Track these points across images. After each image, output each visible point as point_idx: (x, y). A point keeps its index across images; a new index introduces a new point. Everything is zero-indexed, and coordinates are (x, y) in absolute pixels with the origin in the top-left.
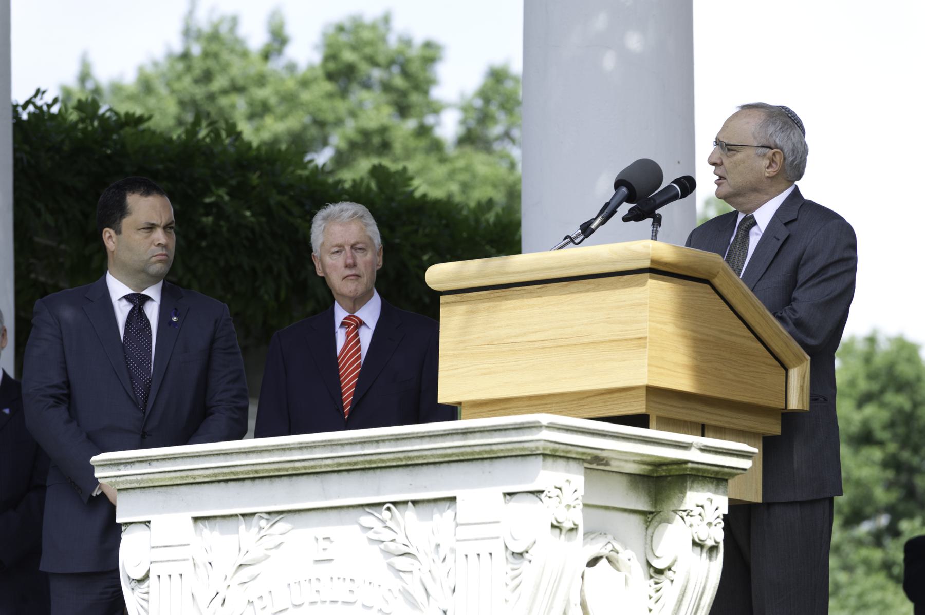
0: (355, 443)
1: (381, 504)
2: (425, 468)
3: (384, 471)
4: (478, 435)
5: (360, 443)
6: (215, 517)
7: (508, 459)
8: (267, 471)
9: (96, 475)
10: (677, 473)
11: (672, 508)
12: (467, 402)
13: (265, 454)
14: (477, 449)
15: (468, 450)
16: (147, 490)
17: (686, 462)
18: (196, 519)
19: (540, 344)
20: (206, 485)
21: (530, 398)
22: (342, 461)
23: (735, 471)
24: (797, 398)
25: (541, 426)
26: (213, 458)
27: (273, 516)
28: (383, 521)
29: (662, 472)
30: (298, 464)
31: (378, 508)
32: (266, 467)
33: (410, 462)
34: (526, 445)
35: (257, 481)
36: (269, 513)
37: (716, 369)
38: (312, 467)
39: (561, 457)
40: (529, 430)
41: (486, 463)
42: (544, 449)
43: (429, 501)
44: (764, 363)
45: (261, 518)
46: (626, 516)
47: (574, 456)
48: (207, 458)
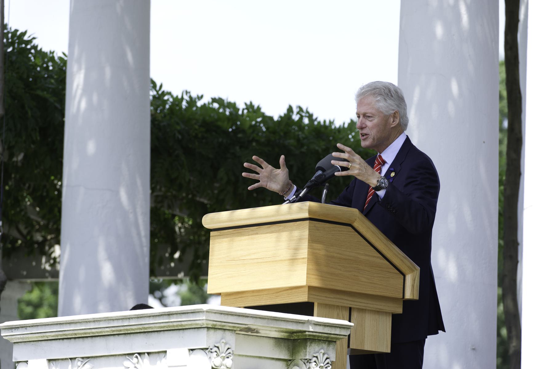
0: (119, 319)
1: (133, 354)
2: (153, 333)
3: (135, 335)
4: (175, 316)
5: (121, 319)
6: (58, 359)
7: (191, 330)
8: (80, 334)
9: (2, 335)
10: (302, 338)
11: (300, 358)
12: (223, 293)
13: (78, 325)
14: (175, 324)
15: (171, 324)
16: (27, 343)
17: (305, 332)
18: (49, 360)
19: (256, 261)
20: (54, 341)
21: (253, 291)
22: (113, 329)
23: (339, 336)
24: (411, 292)
25: (204, 312)
26: (55, 326)
27: (85, 359)
28: (134, 364)
29: (295, 337)
30: (93, 331)
31: (130, 356)
32: (79, 332)
33: (145, 331)
34: (197, 322)
35: (77, 340)
36: (83, 358)
37: (355, 276)
38: (101, 332)
39: (219, 329)
40: (198, 314)
41: (181, 331)
42: (207, 324)
43: (155, 353)
44: (388, 272)
45: (79, 360)
46: (274, 362)
47: (228, 328)
48: (52, 326)
